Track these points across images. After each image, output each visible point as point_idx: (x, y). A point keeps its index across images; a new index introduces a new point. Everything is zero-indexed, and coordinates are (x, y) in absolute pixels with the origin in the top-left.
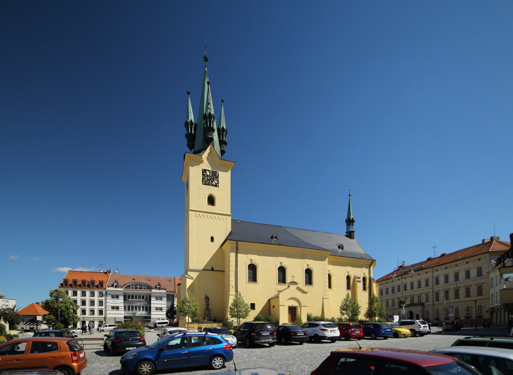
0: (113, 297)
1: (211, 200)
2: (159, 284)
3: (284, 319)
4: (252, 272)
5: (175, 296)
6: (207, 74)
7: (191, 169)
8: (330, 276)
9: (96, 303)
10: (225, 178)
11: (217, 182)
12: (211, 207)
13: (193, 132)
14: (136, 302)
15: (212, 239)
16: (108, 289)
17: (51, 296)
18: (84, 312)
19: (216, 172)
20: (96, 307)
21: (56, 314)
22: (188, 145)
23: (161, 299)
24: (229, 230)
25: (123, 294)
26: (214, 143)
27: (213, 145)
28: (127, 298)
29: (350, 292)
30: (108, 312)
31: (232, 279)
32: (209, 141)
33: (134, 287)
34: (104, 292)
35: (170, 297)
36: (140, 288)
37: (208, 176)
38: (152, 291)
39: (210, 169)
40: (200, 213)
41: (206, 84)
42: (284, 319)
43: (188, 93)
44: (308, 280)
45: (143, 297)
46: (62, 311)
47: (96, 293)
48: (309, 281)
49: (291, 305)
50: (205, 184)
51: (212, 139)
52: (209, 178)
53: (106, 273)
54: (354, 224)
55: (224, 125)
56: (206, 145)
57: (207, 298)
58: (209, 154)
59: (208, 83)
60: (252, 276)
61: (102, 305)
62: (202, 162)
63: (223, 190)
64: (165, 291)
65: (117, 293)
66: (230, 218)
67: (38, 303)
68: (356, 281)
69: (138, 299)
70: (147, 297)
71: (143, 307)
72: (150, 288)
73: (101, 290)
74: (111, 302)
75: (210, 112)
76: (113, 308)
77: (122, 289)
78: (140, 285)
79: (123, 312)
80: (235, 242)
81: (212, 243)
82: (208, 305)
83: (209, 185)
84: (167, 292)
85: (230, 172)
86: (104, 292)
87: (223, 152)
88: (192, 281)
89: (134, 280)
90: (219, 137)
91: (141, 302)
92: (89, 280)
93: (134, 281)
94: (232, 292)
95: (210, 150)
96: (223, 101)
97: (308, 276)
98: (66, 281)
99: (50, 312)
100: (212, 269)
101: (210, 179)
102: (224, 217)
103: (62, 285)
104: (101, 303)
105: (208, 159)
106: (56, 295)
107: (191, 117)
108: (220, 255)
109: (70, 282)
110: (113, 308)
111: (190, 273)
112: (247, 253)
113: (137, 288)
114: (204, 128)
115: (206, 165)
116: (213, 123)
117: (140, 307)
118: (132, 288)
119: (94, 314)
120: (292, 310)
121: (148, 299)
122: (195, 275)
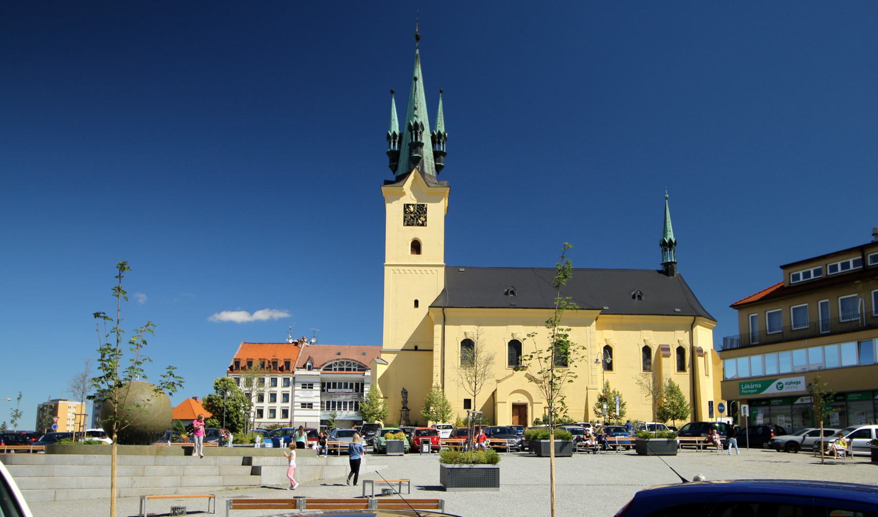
0: (304, 386)
1: (416, 247)
3: (505, 418)
7: (389, 206)
8: (608, 350)
9: (279, 397)
10: (437, 212)
12: (416, 256)
14: (339, 394)
15: (416, 303)
16: (297, 372)
17: (216, 388)
18: (260, 413)
20: (279, 405)
21: (220, 418)
22: (390, 167)
24: (441, 286)
28: (325, 388)
29: (650, 375)
30: (296, 413)
32: (416, 161)
33: (337, 367)
34: (291, 379)
39: (415, 202)
40: (400, 268)
42: (505, 418)
45: (351, 387)
46: (229, 413)
47: (280, 381)
49: (516, 401)
50: (408, 225)
53: (296, 344)
56: (412, 165)
58: (413, 182)
61: (288, 401)
62: (404, 194)
63: (433, 233)
65: (310, 380)
67: (195, 398)
69: (343, 390)
70: (357, 384)
71: (351, 403)
73: (286, 376)
74: (301, 395)
76: (304, 405)
77: (319, 373)
78: (347, 363)
79: (319, 413)
80: (441, 309)
83: (413, 225)
86: (291, 379)
87: (438, 168)
88: (385, 367)
92: (270, 359)
93: (338, 357)
95: (415, 176)
96: (441, 92)
98: (237, 363)
99: (214, 413)
100: (416, 349)
103: (231, 368)
104: (286, 397)
105: (412, 188)
106: (222, 387)
108: (426, 327)
109: (243, 364)
110: (304, 405)
115: (409, 198)
117: (345, 403)
118: (335, 370)
119: (274, 417)
120: (520, 410)
122: (390, 358)
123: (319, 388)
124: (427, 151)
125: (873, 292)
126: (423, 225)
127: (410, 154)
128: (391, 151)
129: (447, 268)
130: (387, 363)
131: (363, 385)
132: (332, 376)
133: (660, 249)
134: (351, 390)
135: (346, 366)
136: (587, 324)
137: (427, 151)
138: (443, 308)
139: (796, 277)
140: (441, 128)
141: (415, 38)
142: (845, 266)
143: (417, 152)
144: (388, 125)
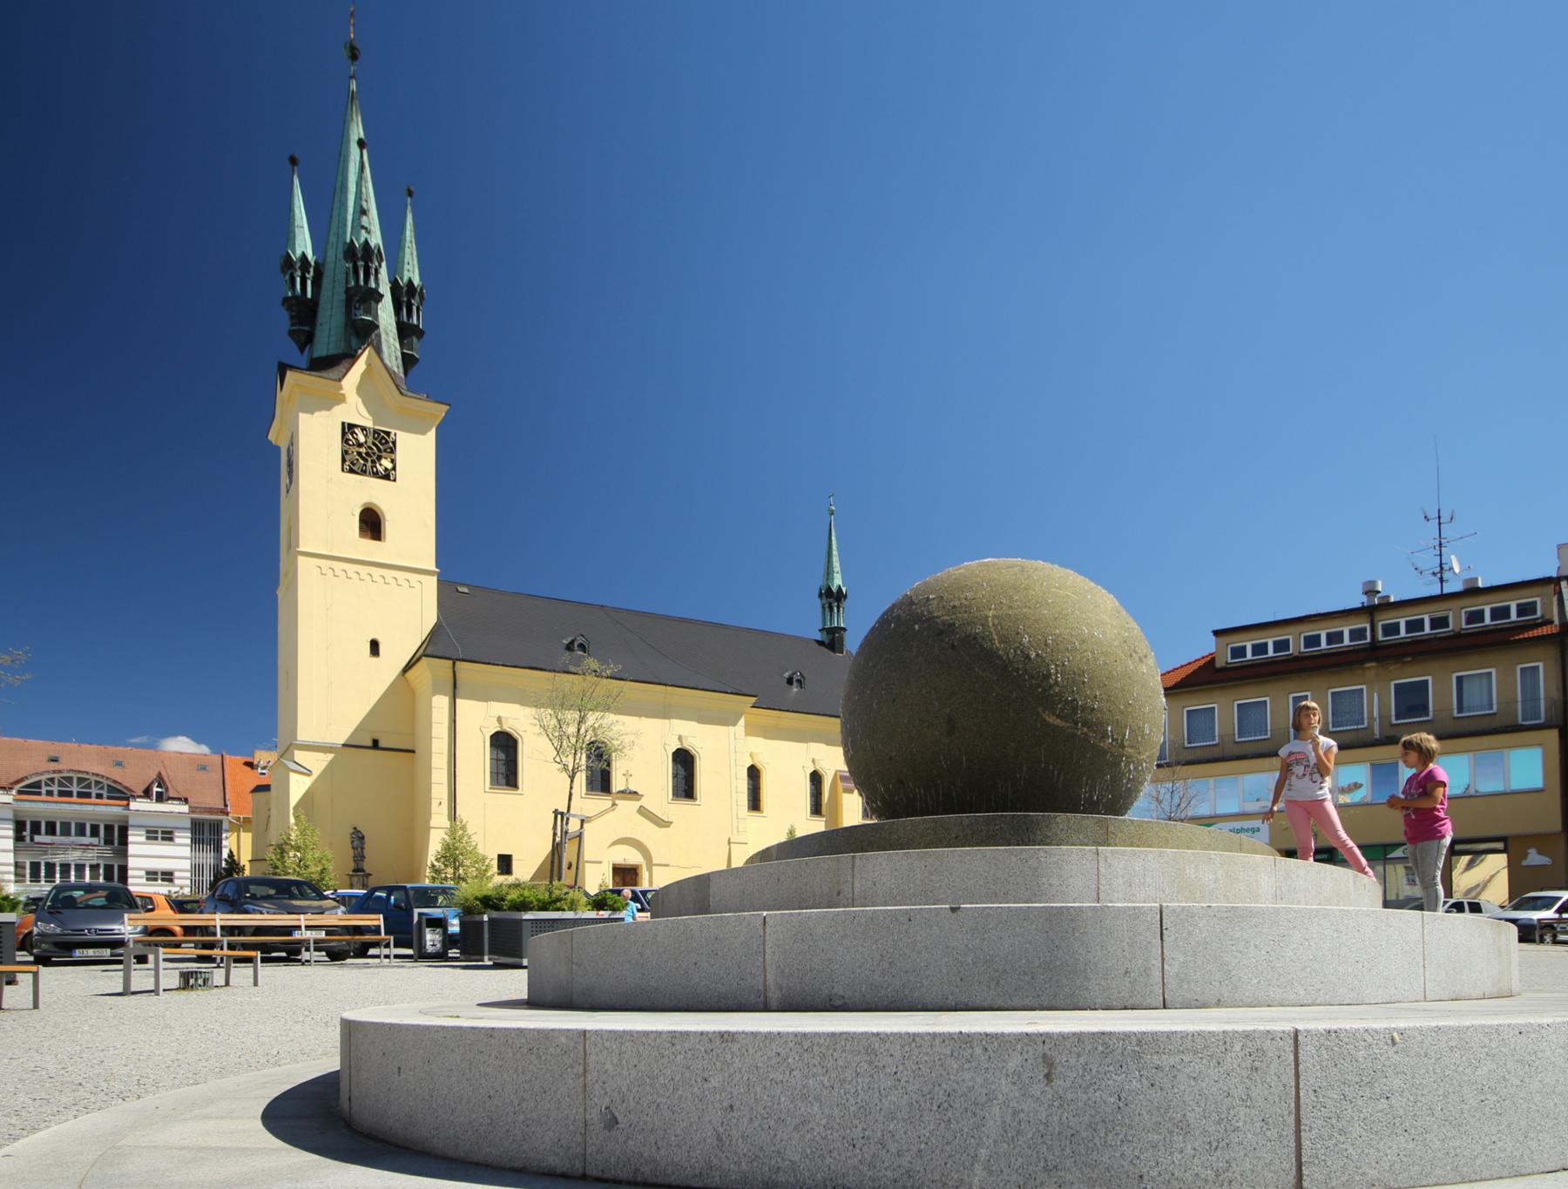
1: (371, 523)
2: (161, 782)
4: (502, 756)
5: (225, 826)
6: (356, 102)
8: (754, 773)
10: (417, 453)
11: (389, 466)
13: (309, 295)
15: (375, 647)
19: (388, 434)
22: (291, 333)
23: (168, 836)
24: (431, 618)
25: (11, 816)
26: (379, 336)
27: (378, 351)
28: (27, 833)
31: (439, 776)
32: (365, 333)
33: (55, 789)
35: (206, 833)
36: (80, 795)
37: (360, 445)
38: (134, 805)
39: (369, 423)
40: (335, 564)
41: (354, 150)
43: (293, 161)
44: (682, 785)
45: (95, 831)
48: (685, 786)
49: (620, 861)
50: (351, 471)
51: (374, 326)
52: (363, 450)
54: (846, 604)
55: (412, 272)
56: (354, 341)
57: (358, 838)
58: (366, 376)
59: (361, 144)
60: (503, 769)
62: (341, 399)
64: (185, 808)
66: (432, 582)
68: (840, 788)
69: (73, 838)
70: (109, 828)
72: (121, 794)
75: (366, 242)
78: (80, 780)
81: (374, 659)
82: (359, 857)
83: (363, 472)
84: (193, 810)
85: (433, 431)
87: (408, 361)
89: (55, 760)
90: (398, 311)
91: (87, 846)
94: (439, 818)
95: (369, 364)
96: (410, 193)
97: (682, 772)
100: (375, 745)
101: (368, 453)
102: (414, 577)
105: (361, 390)
107: (303, 244)
108: (401, 699)
111: (299, 756)
112: (485, 698)
113: (70, 794)
114: (348, 290)
115: (354, 410)
116: (377, 272)
118: (50, 793)
121: (117, 836)
122: (317, 763)
123: (11, 833)
124: (386, 314)
125: (1454, 676)
126: (386, 477)
127: (348, 312)
128: (295, 297)
129: (439, 575)
130: (308, 773)
131: (124, 831)
132: (40, 808)
133: (818, 603)
134: (95, 840)
135: (85, 788)
136: (728, 720)
137: (386, 314)
138: (454, 661)
139: (1239, 652)
140: (412, 272)
141: (346, 53)
142: (1334, 638)
143: (368, 312)
144: (288, 235)
